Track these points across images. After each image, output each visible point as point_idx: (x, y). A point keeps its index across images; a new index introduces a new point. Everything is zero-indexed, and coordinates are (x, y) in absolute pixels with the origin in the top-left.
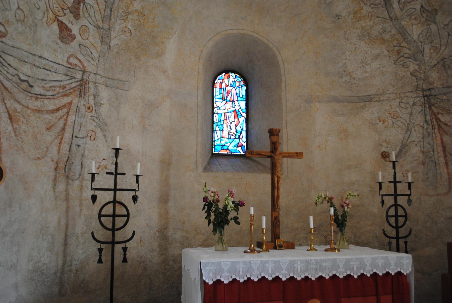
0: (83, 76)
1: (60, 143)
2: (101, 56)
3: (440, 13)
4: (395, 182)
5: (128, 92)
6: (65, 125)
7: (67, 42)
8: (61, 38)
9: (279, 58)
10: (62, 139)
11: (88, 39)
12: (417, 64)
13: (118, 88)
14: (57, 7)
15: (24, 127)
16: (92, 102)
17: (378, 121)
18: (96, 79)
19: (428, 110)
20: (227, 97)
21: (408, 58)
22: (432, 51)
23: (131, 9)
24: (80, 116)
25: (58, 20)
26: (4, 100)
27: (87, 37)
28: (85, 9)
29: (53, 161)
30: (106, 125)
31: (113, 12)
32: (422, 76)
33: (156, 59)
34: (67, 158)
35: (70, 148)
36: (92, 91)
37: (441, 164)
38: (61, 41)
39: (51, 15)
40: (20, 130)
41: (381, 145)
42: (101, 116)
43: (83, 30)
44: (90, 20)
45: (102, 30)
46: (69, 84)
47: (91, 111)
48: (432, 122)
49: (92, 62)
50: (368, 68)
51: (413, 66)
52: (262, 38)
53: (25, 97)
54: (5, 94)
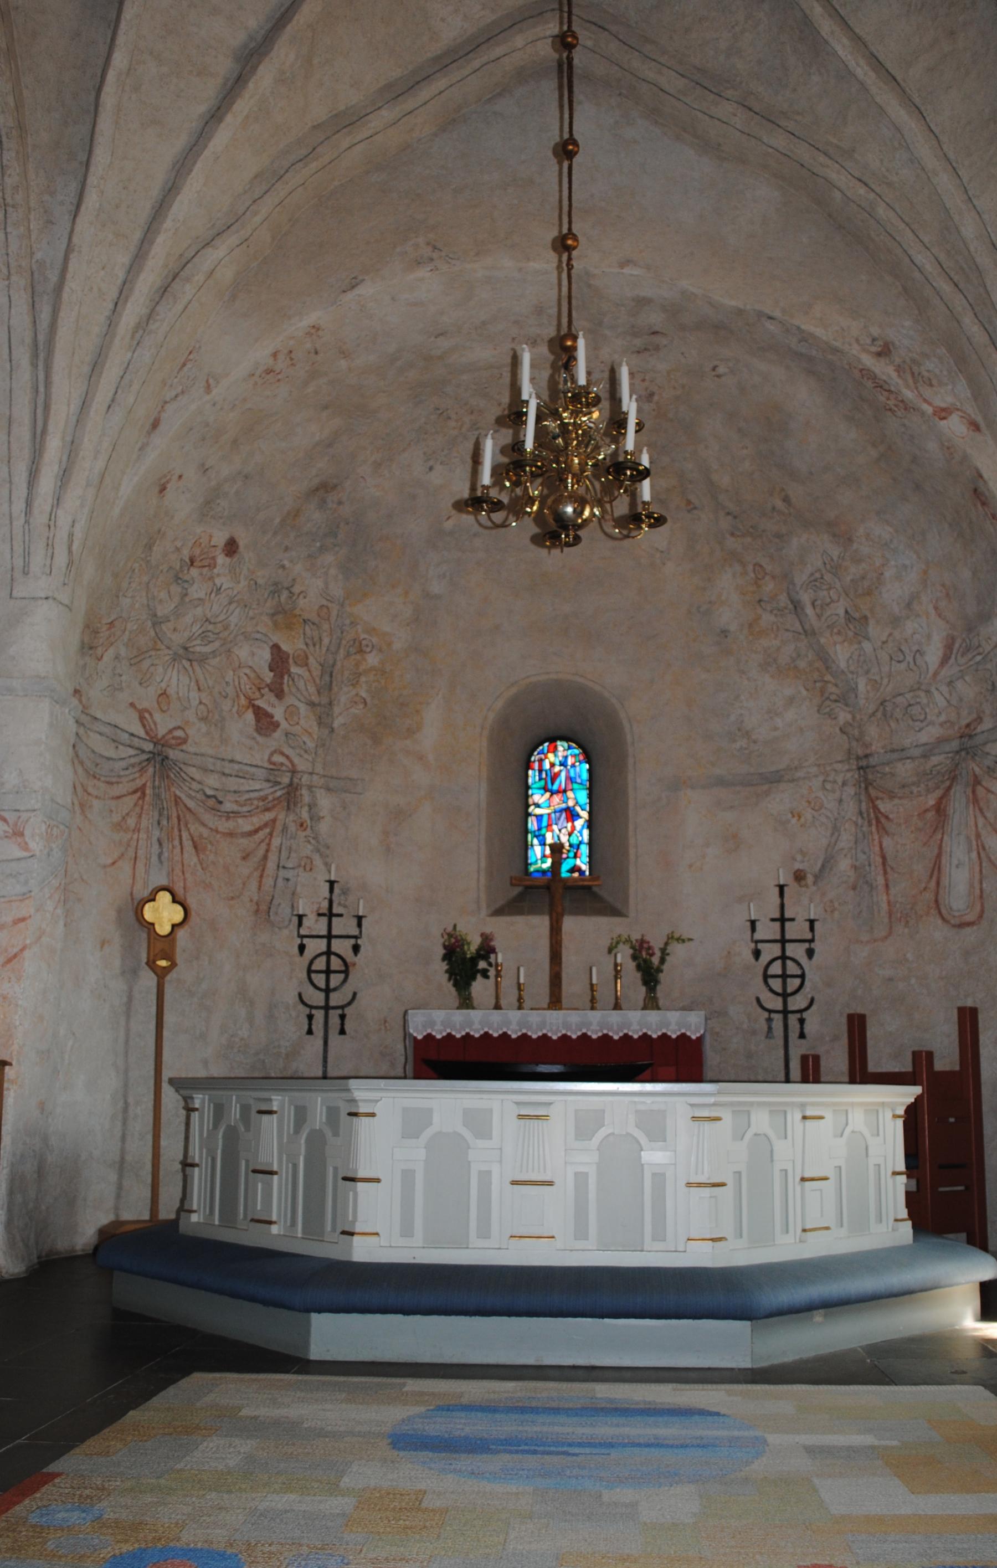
0: (292, 779)
1: (261, 876)
3: (872, 622)
4: (782, 920)
6: (267, 851)
8: (258, 730)
9: (622, 715)
10: (263, 870)
12: (850, 712)
13: (345, 791)
15: (212, 857)
16: (305, 815)
17: (790, 816)
18: (311, 781)
19: (863, 792)
20: (553, 784)
21: (836, 701)
22: (869, 688)
25: (254, 706)
28: (291, 682)
30: (328, 848)
32: (856, 732)
37: (879, 887)
39: (243, 701)
41: (794, 859)
43: (291, 712)
44: (299, 695)
47: (305, 830)
48: (868, 815)
49: (306, 756)
50: (779, 722)
51: (844, 716)
52: (590, 684)
54: (188, 816)
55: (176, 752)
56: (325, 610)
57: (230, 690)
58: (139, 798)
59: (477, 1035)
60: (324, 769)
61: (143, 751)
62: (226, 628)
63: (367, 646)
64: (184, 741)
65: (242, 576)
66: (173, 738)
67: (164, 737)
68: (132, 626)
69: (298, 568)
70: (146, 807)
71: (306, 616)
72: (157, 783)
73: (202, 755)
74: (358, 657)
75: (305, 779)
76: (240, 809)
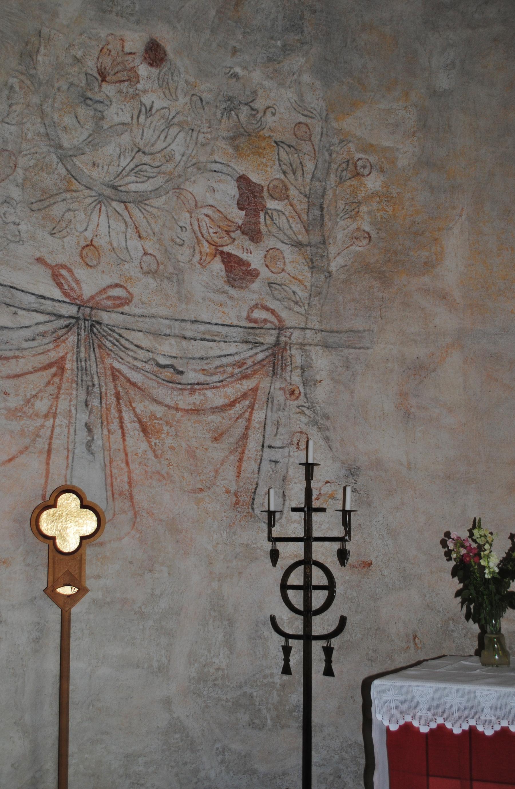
0: (278, 337)
2: (313, 293)
5: (370, 351)
6: (247, 428)
7: (244, 285)
8: (231, 282)
11: (283, 270)
13: (348, 347)
14: (216, 233)
16: (296, 380)
23: (363, 195)
24: (275, 409)
25: (222, 253)
26: (130, 403)
27: (282, 267)
28: (269, 221)
29: (228, 492)
30: (328, 418)
31: (325, 210)
33: (424, 275)
34: (254, 486)
35: (259, 468)
36: (298, 360)
38: (233, 286)
39: (206, 248)
40: (163, 446)
42: (318, 403)
43: (272, 257)
44: (281, 236)
45: (309, 248)
46: (251, 357)
47: (297, 398)
49: (297, 308)
53: (170, 392)
54: (132, 393)
55: (113, 315)
56: (304, 128)
57: (187, 236)
58: (55, 375)
59: (489, 733)
60: (320, 322)
61: (60, 316)
62: (169, 159)
63: (364, 167)
65: (179, 91)
66: (109, 298)
67: (93, 297)
69: (257, 76)
70: (65, 385)
71: (278, 137)
72: (83, 355)
74: (354, 182)
75: (296, 336)
76: (208, 379)
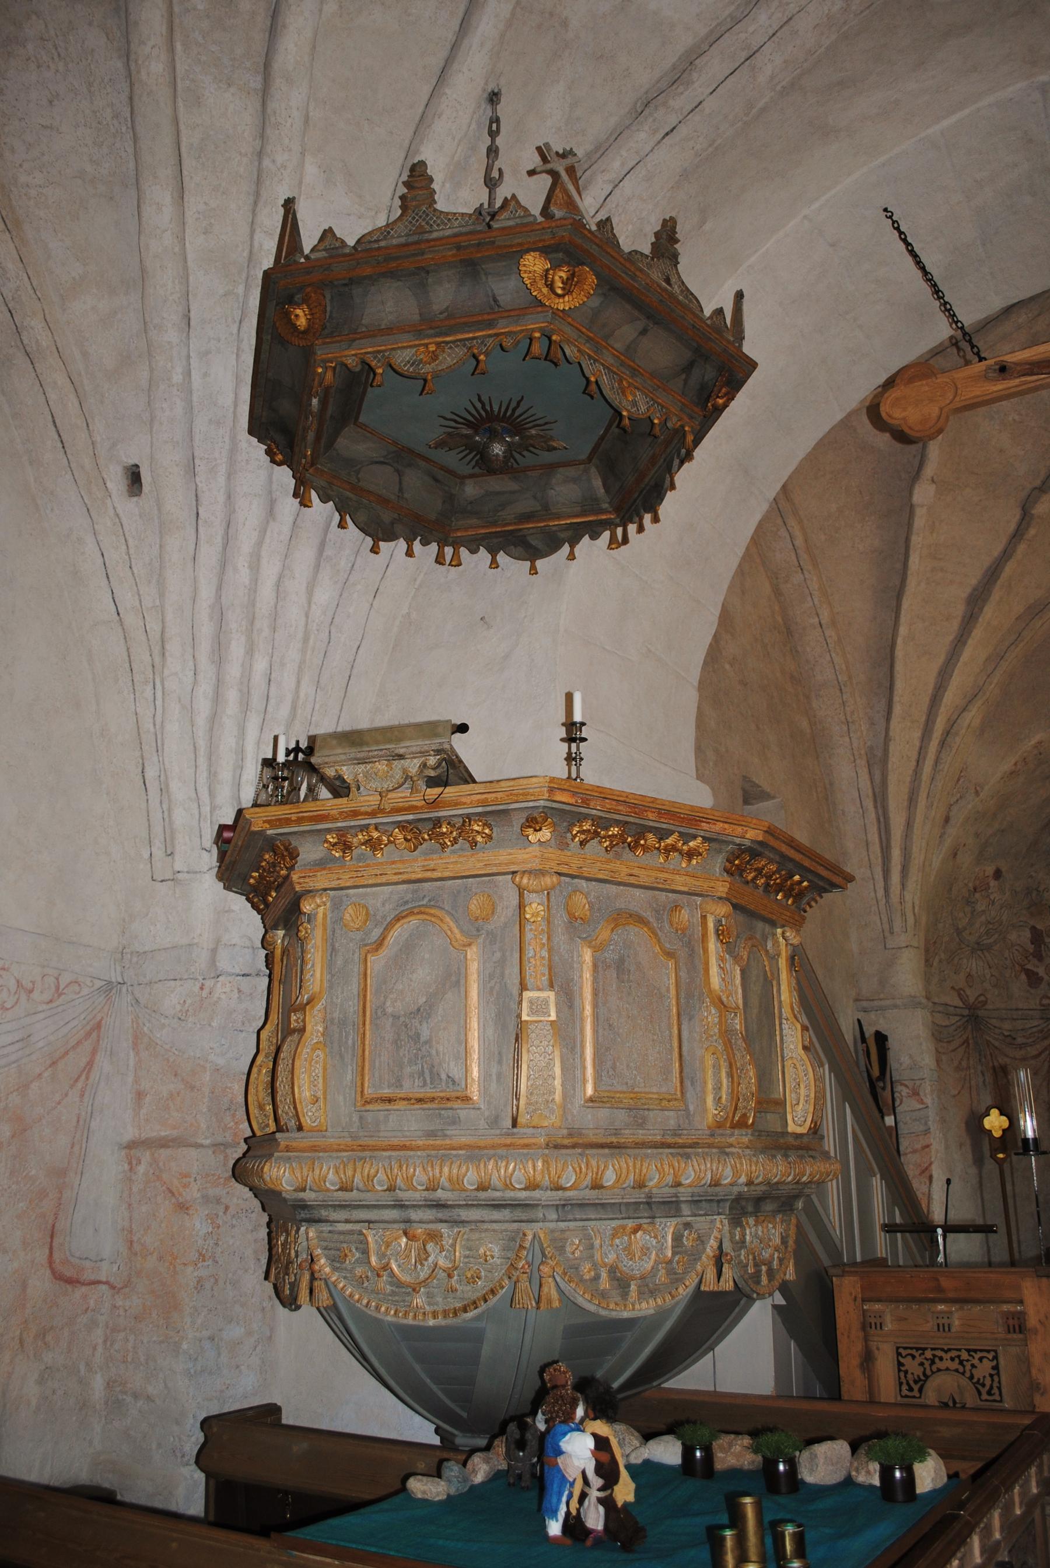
8: (1030, 985)
61: (963, 1016)
64: (985, 1003)
68: (946, 939)
73: (998, 1009)
